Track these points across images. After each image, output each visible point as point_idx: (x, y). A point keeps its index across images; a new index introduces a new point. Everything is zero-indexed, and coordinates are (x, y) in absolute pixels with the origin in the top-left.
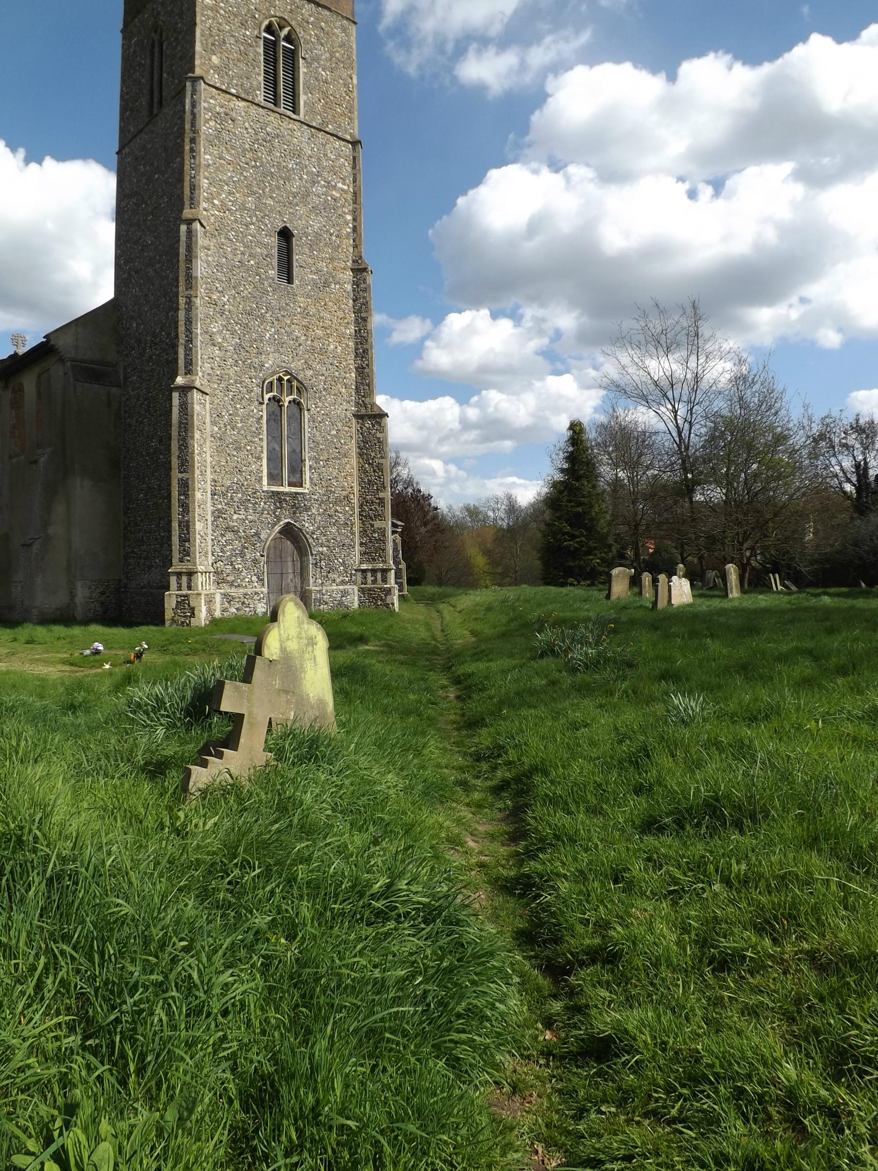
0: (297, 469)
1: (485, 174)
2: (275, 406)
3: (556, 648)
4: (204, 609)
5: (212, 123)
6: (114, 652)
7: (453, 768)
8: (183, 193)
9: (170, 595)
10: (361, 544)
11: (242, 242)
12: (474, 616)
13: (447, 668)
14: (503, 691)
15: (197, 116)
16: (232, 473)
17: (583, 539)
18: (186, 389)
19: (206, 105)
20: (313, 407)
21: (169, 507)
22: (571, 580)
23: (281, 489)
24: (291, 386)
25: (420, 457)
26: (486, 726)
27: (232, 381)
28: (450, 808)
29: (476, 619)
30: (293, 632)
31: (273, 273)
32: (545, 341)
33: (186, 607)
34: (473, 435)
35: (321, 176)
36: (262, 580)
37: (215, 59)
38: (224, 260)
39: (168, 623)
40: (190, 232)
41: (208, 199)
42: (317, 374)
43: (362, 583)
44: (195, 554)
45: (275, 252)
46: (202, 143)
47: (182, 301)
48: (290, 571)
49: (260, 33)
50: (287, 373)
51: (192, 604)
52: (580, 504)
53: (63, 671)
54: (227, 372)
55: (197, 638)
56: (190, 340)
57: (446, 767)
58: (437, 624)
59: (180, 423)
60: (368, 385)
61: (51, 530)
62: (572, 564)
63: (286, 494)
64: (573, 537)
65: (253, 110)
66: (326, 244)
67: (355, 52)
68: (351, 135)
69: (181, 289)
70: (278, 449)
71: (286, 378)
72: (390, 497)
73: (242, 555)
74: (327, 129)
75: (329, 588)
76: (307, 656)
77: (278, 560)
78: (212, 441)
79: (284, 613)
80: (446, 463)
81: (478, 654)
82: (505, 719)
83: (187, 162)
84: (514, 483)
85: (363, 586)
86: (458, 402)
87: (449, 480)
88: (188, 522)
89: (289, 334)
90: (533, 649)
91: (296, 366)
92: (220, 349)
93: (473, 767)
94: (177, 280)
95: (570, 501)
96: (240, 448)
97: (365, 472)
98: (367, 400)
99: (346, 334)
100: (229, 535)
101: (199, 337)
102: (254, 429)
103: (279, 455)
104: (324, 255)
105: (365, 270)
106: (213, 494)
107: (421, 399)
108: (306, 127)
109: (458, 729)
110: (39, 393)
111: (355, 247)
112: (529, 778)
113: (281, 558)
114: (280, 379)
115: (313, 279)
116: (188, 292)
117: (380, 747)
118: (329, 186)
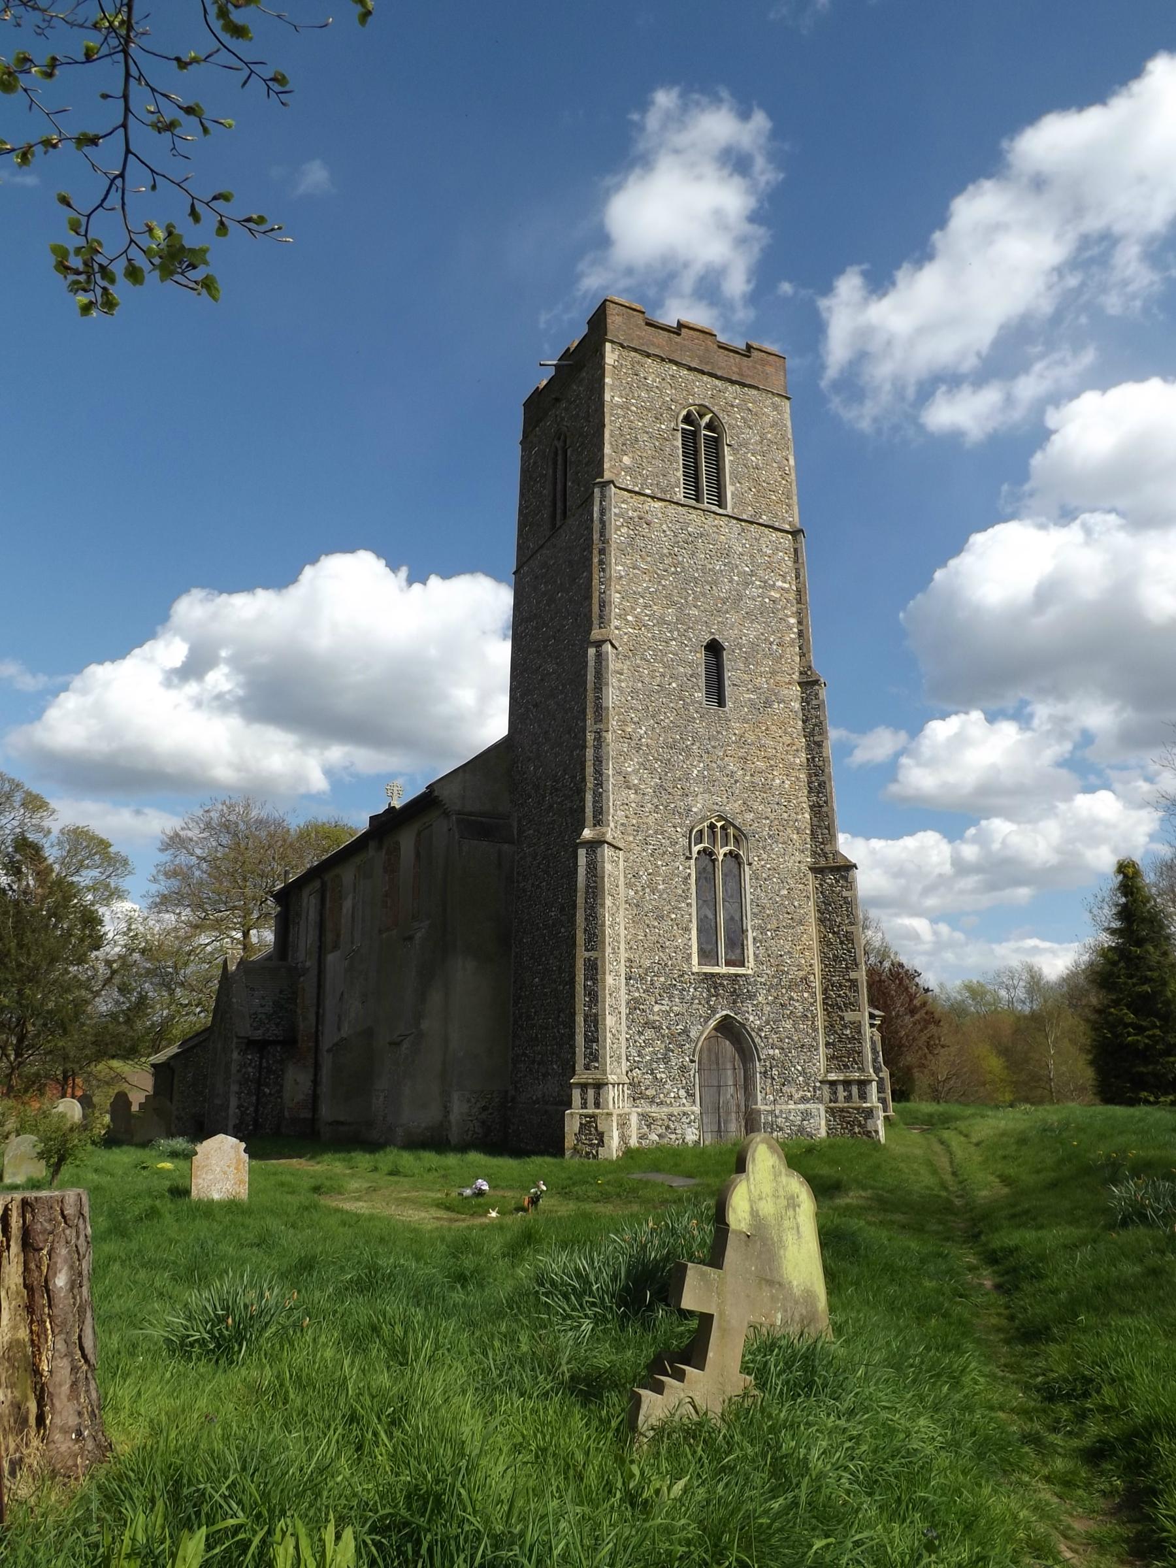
0: (736, 942)
1: (966, 540)
2: (706, 860)
3: (1149, 1212)
4: (616, 1134)
5: (624, 530)
6: (500, 1193)
7: (1012, 1410)
8: (591, 611)
9: (571, 1114)
10: (827, 1044)
11: (662, 661)
12: (1000, 1153)
13: (973, 1238)
14: (1072, 1281)
15: (607, 524)
16: (652, 950)
17: (1157, 1032)
18: (595, 845)
19: (617, 511)
20: (756, 860)
21: (573, 996)
22: (1143, 1094)
23: (716, 970)
24: (727, 835)
25: (897, 915)
26: (1054, 1340)
27: (651, 832)
28: (1020, 1483)
29: (1004, 1157)
30: (767, 1188)
31: (699, 695)
32: (1068, 746)
33: (593, 1132)
34: (970, 882)
35: (756, 575)
36: (693, 1095)
37: (626, 460)
38: (640, 684)
39: (568, 1153)
40: (599, 655)
41: (620, 616)
42: (759, 817)
43: (831, 1101)
44: (605, 1059)
45: (702, 670)
46: (613, 552)
47: (590, 737)
48: (730, 1082)
49: (677, 425)
50: (721, 818)
51: (600, 1129)
52: (1146, 980)
53: (437, 1218)
54: (645, 820)
55: (610, 1177)
56: (599, 784)
57: (1002, 1408)
58: (944, 1162)
59: (588, 886)
60: (828, 828)
61: (425, 1025)
62: (1142, 1069)
63: (723, 976)
64: (1140, 1029)
65: (672, 510)
66: (765, 656)
67: (790, 431)
68: (790, 523)
69: (589, 722)
70: (711, 916)
71: (719, 824)
72: (865, 978)
73: (666, 1060)
74: (761, 521)
75: (784, 1107)
76: (786, 1223)
77: (714, 1067)
78: (626, 909)
79: (754, 1160)
80: (934, 921)
81: (1021, 1217)
82: (1084, 1331)
83: (595, 576)
84: (1036, 948)
85: (832, 1105)
86: (945, 837)
87: (940, 945)
88: (596, 1015)
89: (721, 769)
90: (1107, 1211)
91: (732, 808)
92: (636, 793)
93: (1044, 1411)
94: (584, 712)
95: (1131, 977)
96: (662, 917)
97: (829, 944)
98: (828, 848)
99: (796, 765)
100: (649, 1033)
101: (611, 779)
102: (680, 892)
103: (713, 924)
104: (763, 669)
105: (816, 682)
106: (629, 978)
107: (895, 835)
108: (735, 522)
109: (1007, 1342)
110: (418, 855)
111: (802, 655)
112: (1148, 1440)
113: (718, 1064)
114: (712, 827)
115: (750, 700)
116: (598, 726)
117: (898, 1368)
118: (766, 585)
